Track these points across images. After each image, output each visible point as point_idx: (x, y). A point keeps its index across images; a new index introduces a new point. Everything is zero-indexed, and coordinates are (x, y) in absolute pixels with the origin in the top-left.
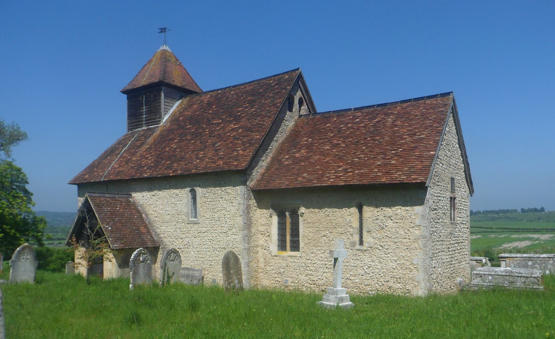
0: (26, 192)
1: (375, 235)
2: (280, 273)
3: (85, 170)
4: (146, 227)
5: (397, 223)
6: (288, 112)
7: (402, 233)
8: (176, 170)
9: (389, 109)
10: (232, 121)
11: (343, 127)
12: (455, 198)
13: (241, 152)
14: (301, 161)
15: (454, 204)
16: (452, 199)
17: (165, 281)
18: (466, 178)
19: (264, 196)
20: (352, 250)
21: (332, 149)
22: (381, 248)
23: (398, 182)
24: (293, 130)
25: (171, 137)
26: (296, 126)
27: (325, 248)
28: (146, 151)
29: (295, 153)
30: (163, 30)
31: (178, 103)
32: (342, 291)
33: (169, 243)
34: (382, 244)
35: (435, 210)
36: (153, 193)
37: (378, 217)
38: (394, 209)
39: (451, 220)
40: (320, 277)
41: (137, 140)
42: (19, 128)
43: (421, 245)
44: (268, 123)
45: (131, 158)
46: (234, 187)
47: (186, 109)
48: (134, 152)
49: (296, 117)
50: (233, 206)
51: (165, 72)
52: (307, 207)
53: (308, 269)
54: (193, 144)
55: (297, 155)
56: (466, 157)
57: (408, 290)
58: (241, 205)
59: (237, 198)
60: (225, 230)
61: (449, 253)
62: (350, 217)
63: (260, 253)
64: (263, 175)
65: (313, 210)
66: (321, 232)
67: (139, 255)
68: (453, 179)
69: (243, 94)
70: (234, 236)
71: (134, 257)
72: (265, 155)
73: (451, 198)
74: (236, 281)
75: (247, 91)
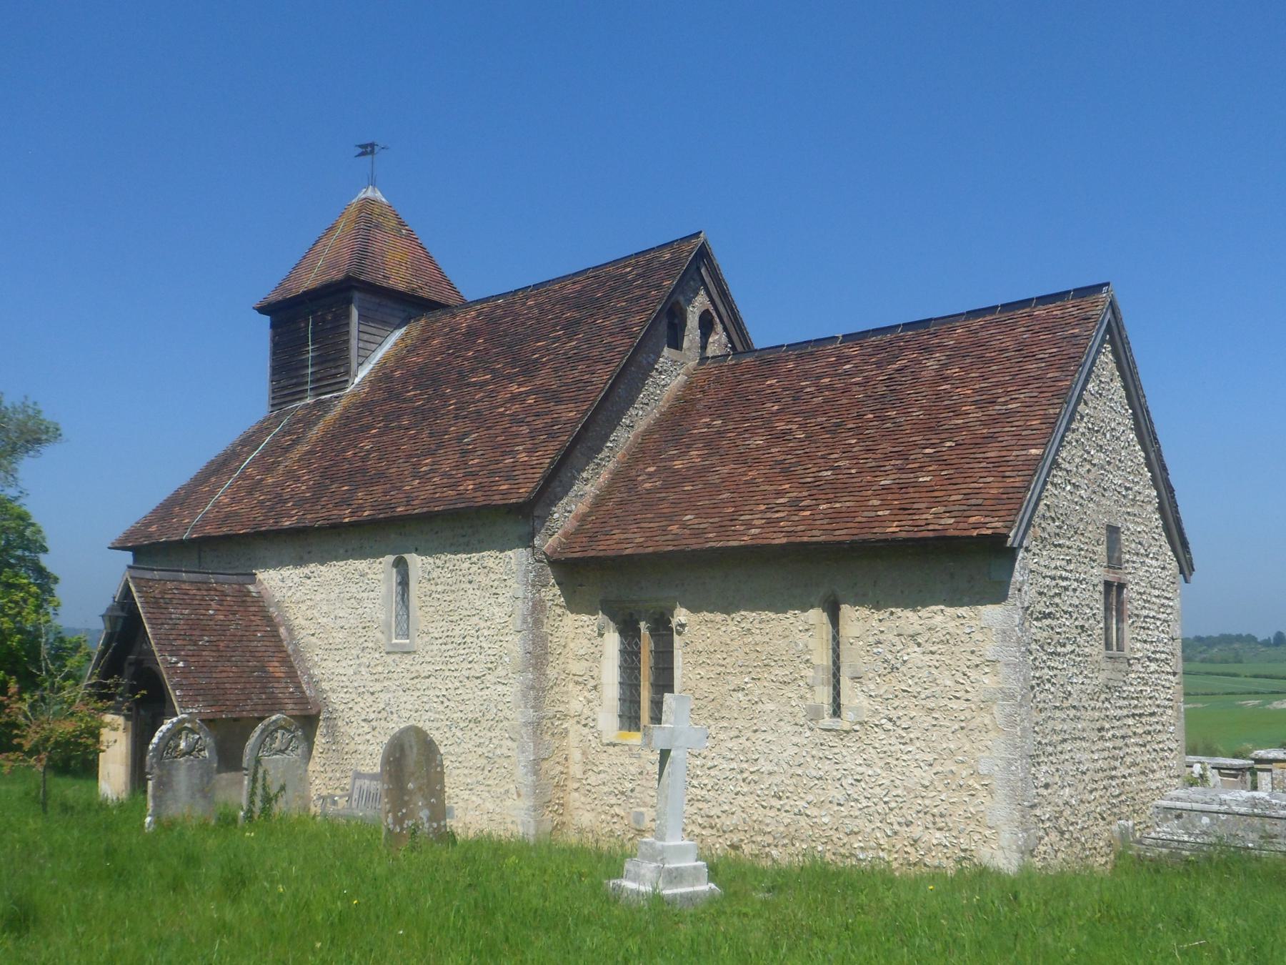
0: (40, 572)
1: (872, 687)
2: (623, 793)
3: (155, 511)
4: (286, 661)
5: (932, 653)
6: (666, 349)
7: (948, 683)
8: (361, 508)
9: (935, 335)
10: (517, 375)
11: (807, 386)
12: (1121, 586)
13: (523, 457)
14: (685, 479)
15: (1120, 603)
16: (1114, 590)
17: (257, 810)
18: (1166, 528)
19: (586, 576)
20: (811, 729)
21: (769, 447)
22: (889, 726)
23: (931, 534)
24: (678, 399)
25: (364, 421)
26: (688, 386)
27: (739, 724)
28: (299, 461)
29: (672, 459)
30: (368, 149)
31: (398, 334)
32: (680, 852)
33: (342, 707)
34: (893, 714)
35: (1049, 616)
36: (306, 570)
37: (882, 637)
38: (924, 612)
39: (1108, 646)
40: (726, 807)
41: (285, 433)
42: (39, 412)
43: (1000, 720)
44: (602, 377)
45: (262, 480)
46: (501, 551)
47: (412, 350)
48: (273, 463)
49: (692, 364)
50: (500, 605)
51: (363, 254)
52: (694, 609)
53: (695, 782)
54: (411, 438)
55: (678, 464)
56: (1164, 468)
57: (964, 851)
58: (519, 602)
59: (508, 583)
60: (478, 669)
61: (1100, 745)
62: (806, 636)
63: (571, 734)
64: (583, 518)
65: (709, 616)
67: (176, 733)
68: (1113, 531)
69: (554, 305)
70: (500, 688)
71: (160, 739)
72: (592, 466)
73: (1108, 584)
74: (424, 814)
75: (565, 298)
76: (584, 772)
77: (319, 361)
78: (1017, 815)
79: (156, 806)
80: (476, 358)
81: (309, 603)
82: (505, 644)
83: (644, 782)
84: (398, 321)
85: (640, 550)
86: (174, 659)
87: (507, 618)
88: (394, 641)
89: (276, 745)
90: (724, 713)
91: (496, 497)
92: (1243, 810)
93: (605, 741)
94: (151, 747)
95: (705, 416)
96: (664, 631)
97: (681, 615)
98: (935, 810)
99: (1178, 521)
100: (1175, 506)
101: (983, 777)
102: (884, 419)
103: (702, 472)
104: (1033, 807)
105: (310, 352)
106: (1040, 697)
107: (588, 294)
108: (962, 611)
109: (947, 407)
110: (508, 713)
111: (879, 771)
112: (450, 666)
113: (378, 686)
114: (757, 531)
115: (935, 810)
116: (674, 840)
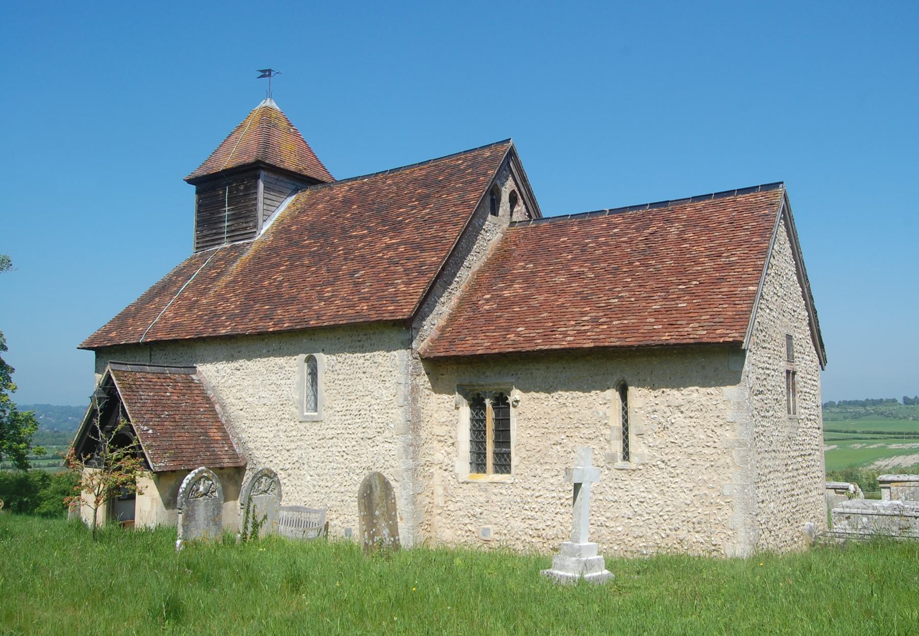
1: (651, 440)
2: (474, 516)
3: (111, 322)
4: (221, 428)
5: (691, 417)
6: (490, 215)
7: (702, 437)
8: (281, 321)
9: (673, 211)
11: (589, 243)
12: (794, 373)
13: (402, 288)
14: (514, 303)
15: (794, 384)
16: (791, 374)
19: (442, 368)
20: (609, 469)
21: (570, 283)
22: (662, 465)
23: (692, 341)
25: (273, 261)
26: (505, 240)
28: (226, 287)
29: (501, 289)
30: (266, 73)
33: (264, 460)
34: (665, 458)
35: (761, 392)
36: (236, 364)
37: (657, 408)
38: (685, 391)
39: (789, 413)
40: (549, 523)
44: (452, 235)
45: (197, 301)
46: (388, 352)
47: (303, 211)
48: (205, 289)
49: (506, 226)
50: (387, 388)
51: (266, 145)
52: (525, 390)
53: (526, 507)
54: (313, 273)
58: (402, 387)
59: (393, 373)
63: (435, 476)
64: (443, 330)
65: (535, 395)
66: (550, 436)
67: (197, 481)
68: (789, 337)
69: (407, 184)
70: (386, 445)
71: (188, 484)
72: (446, 294)
73: (788, 372)
74: (386, 532)
75: (416, 180)
76: (445, 502)
77: (233, 218)
78: (749, 521)
79: (185, 532)
80: (353, 218)
81: (238, 387)
82: (390, 415)
83: (490, 508)
84: (290, 191)
85: (489, 351)
86: (146, 428)
87: (392, 397)
88: (306, 414)
89: (262, 487)
90: (547, 460)
91: (386, 315)
92: (889, 512)
93: (460, 481)
94: (181, 490)
95: (520, 261)
96: (502, 403)
97: (516, 394)
98: (694, 520)
99: (819, 332)
100: (817, 322)
101: (727, 497)
102: (648, 266)
103: (525, 299)
104: (757, 515)
105: (227, 211)
106: (759, 444)
107: (433, 178)
108: (710, 390)
109: (689, 259)
110: (393, 463)
111: (656, 495)
112: (348, 431)
113: (293, 445)
114: (572, 338)
115: (694, 520)
116: (584, 543)
